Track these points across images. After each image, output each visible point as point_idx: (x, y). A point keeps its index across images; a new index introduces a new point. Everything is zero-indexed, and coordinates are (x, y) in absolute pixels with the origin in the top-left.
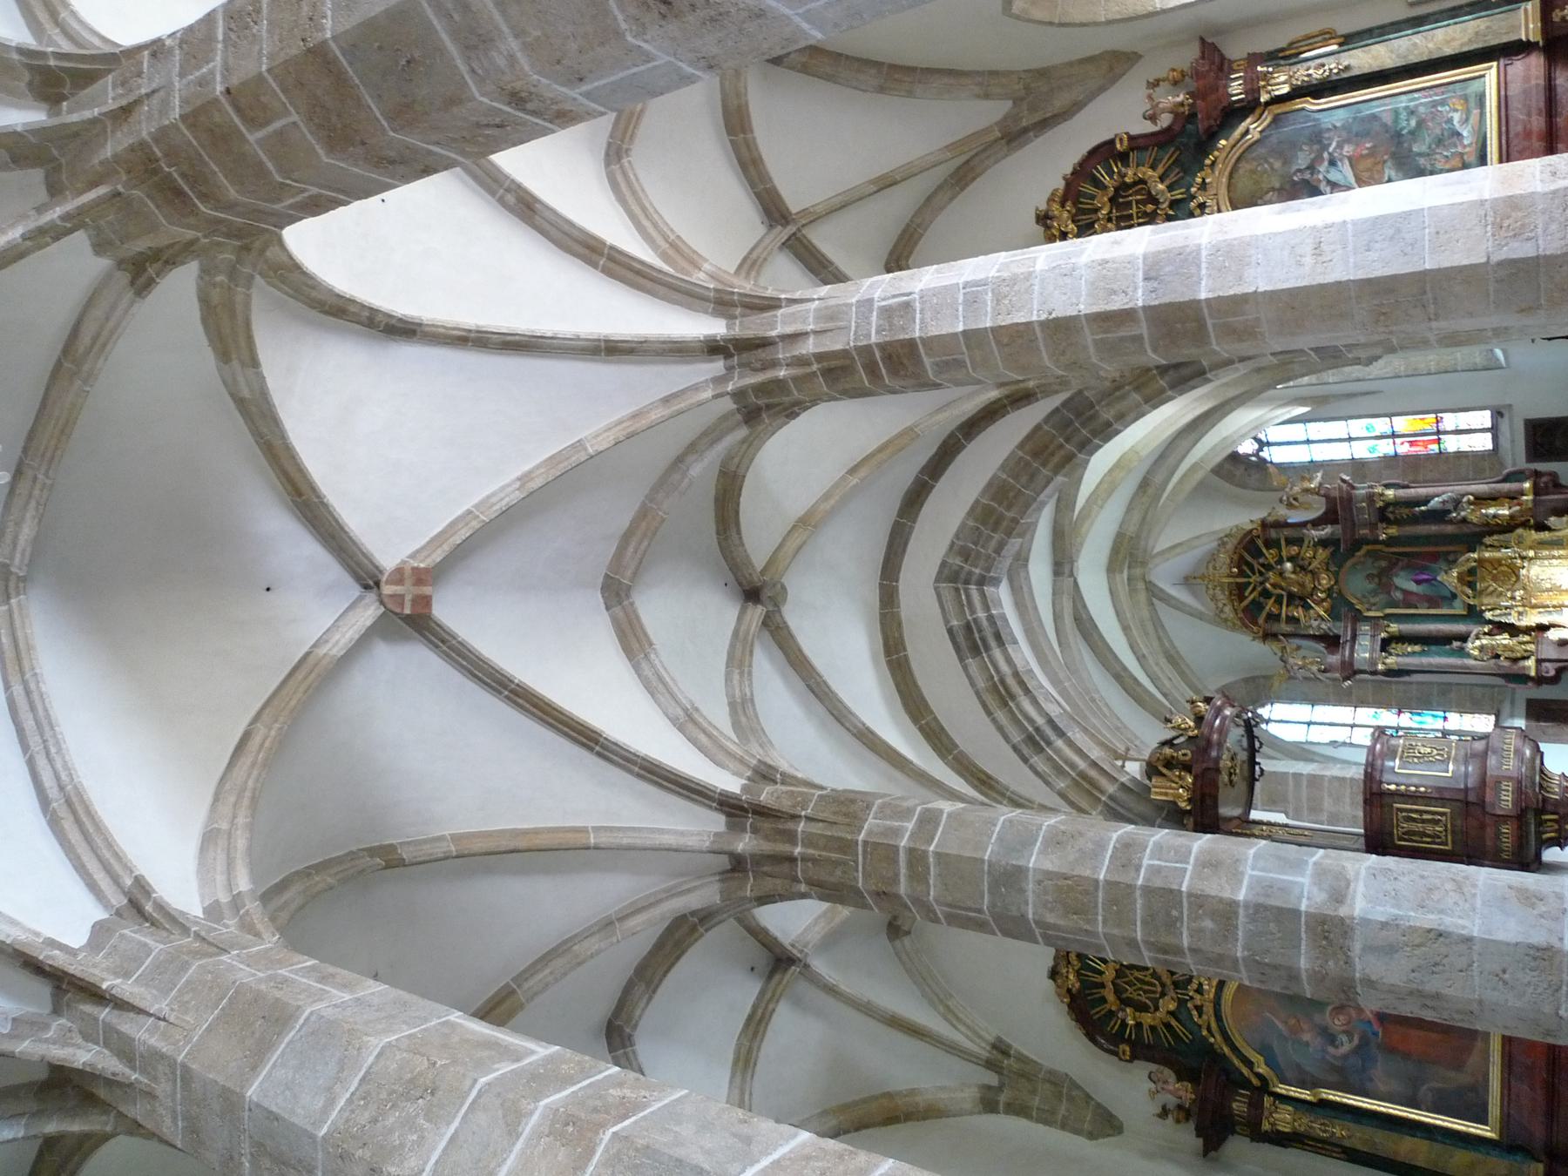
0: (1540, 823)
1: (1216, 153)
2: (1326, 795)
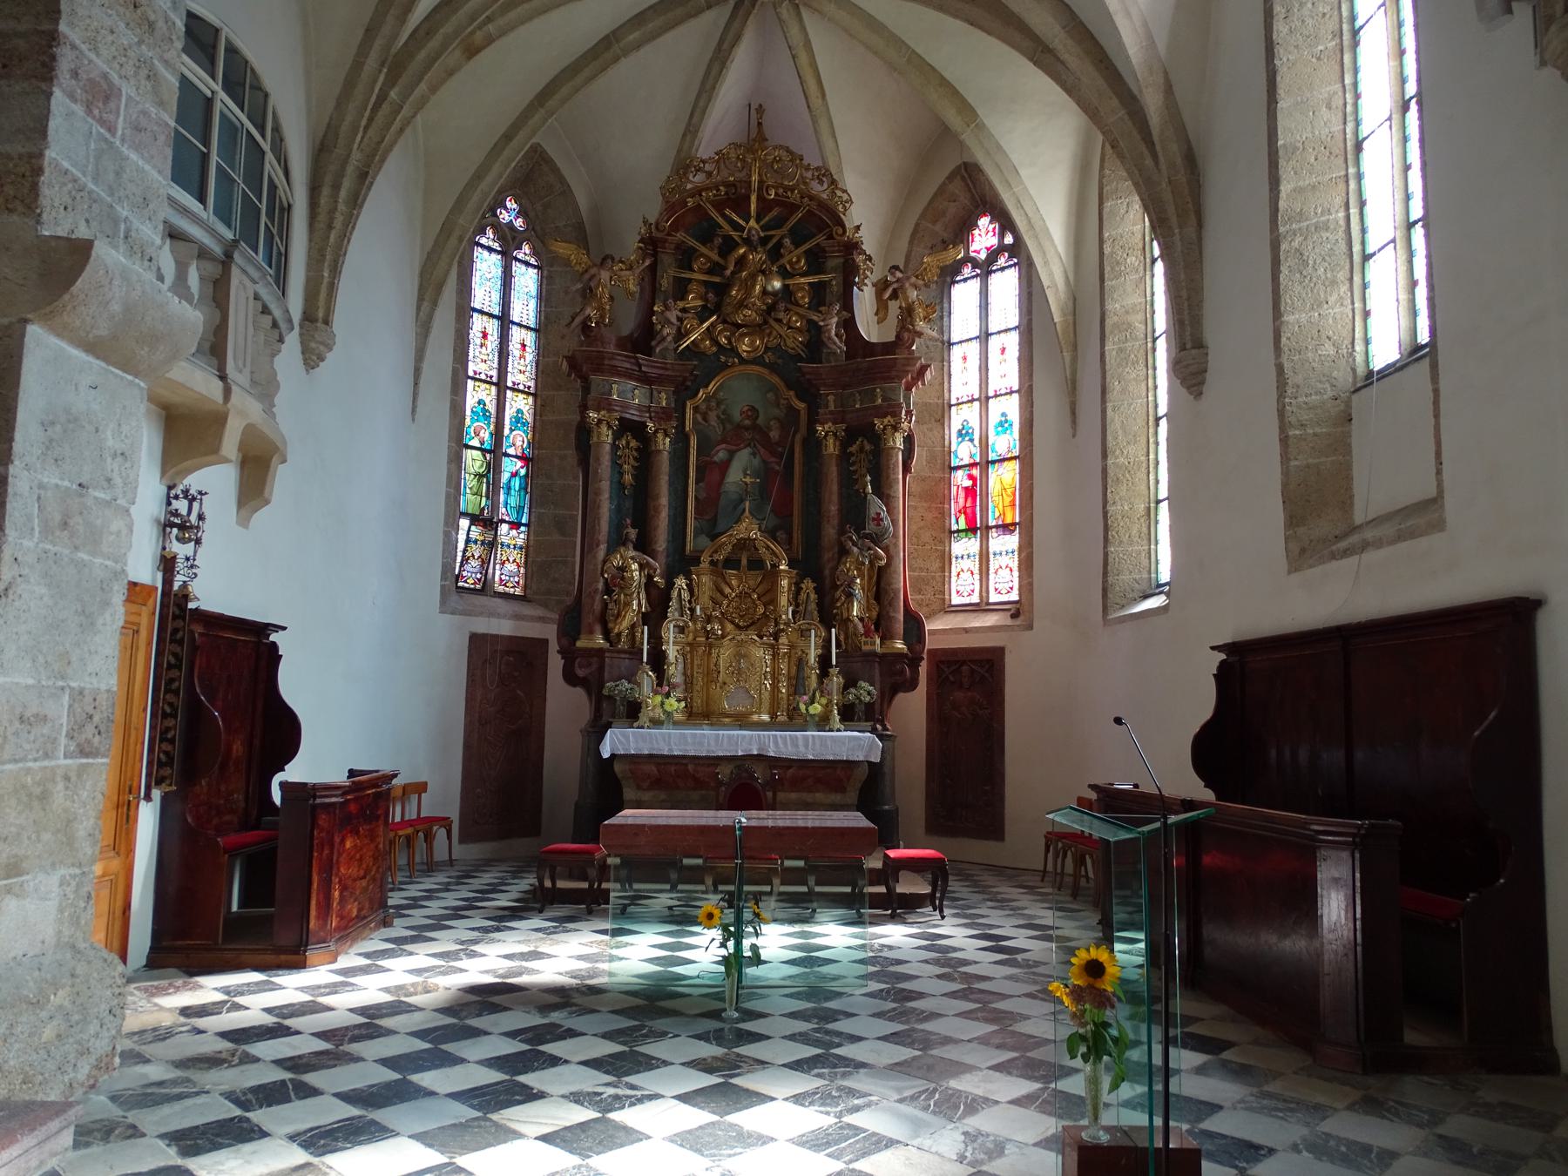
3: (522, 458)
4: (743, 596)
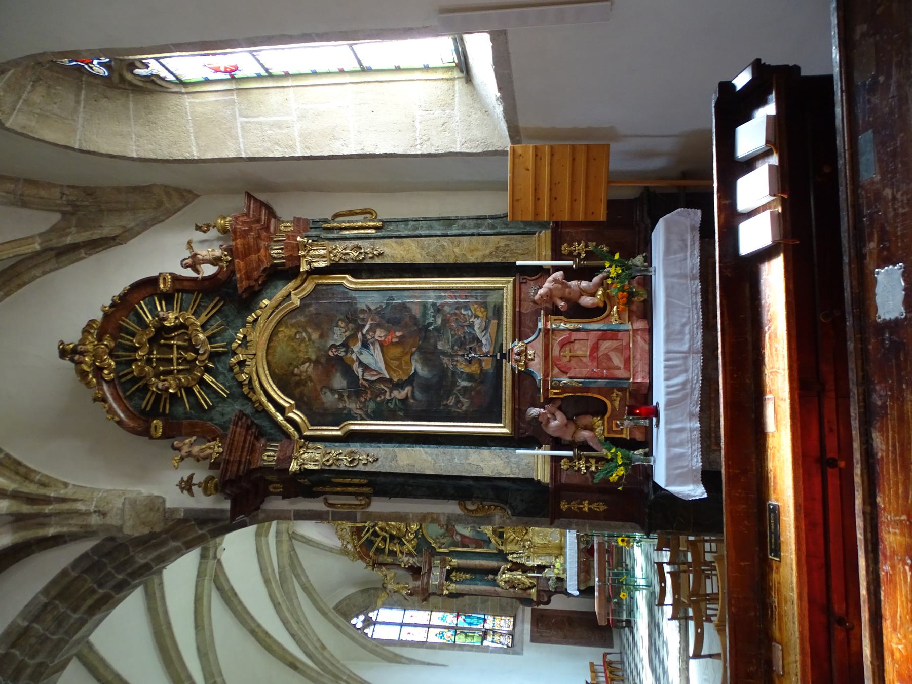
1: (259, 312)
3: (458, 616)
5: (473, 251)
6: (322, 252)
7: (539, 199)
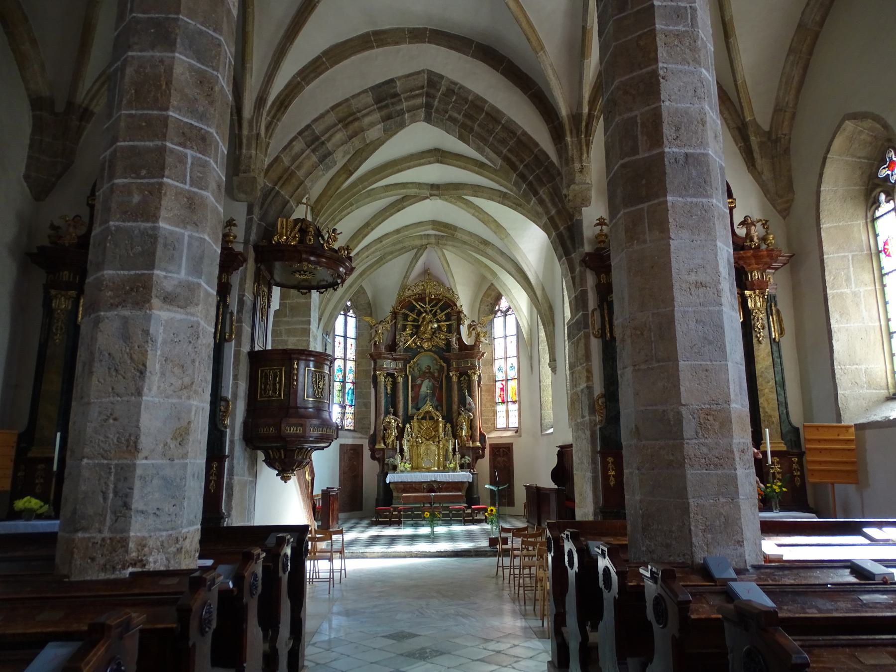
0: (278, 449)
2: (298, 338)
4: (428, 429)
5: (767, 401)
6: (759, 305)
7: (819, 442)
